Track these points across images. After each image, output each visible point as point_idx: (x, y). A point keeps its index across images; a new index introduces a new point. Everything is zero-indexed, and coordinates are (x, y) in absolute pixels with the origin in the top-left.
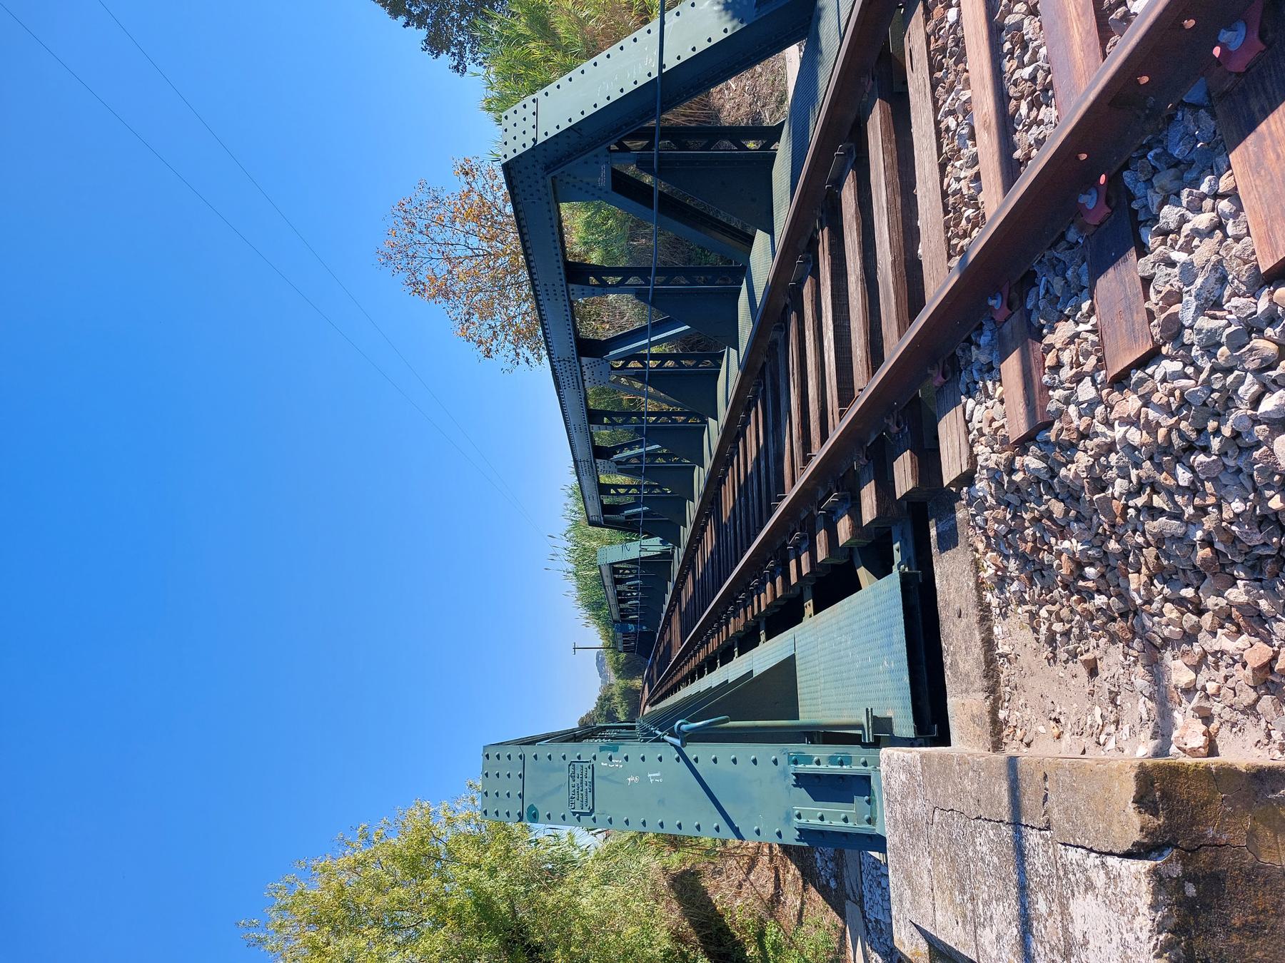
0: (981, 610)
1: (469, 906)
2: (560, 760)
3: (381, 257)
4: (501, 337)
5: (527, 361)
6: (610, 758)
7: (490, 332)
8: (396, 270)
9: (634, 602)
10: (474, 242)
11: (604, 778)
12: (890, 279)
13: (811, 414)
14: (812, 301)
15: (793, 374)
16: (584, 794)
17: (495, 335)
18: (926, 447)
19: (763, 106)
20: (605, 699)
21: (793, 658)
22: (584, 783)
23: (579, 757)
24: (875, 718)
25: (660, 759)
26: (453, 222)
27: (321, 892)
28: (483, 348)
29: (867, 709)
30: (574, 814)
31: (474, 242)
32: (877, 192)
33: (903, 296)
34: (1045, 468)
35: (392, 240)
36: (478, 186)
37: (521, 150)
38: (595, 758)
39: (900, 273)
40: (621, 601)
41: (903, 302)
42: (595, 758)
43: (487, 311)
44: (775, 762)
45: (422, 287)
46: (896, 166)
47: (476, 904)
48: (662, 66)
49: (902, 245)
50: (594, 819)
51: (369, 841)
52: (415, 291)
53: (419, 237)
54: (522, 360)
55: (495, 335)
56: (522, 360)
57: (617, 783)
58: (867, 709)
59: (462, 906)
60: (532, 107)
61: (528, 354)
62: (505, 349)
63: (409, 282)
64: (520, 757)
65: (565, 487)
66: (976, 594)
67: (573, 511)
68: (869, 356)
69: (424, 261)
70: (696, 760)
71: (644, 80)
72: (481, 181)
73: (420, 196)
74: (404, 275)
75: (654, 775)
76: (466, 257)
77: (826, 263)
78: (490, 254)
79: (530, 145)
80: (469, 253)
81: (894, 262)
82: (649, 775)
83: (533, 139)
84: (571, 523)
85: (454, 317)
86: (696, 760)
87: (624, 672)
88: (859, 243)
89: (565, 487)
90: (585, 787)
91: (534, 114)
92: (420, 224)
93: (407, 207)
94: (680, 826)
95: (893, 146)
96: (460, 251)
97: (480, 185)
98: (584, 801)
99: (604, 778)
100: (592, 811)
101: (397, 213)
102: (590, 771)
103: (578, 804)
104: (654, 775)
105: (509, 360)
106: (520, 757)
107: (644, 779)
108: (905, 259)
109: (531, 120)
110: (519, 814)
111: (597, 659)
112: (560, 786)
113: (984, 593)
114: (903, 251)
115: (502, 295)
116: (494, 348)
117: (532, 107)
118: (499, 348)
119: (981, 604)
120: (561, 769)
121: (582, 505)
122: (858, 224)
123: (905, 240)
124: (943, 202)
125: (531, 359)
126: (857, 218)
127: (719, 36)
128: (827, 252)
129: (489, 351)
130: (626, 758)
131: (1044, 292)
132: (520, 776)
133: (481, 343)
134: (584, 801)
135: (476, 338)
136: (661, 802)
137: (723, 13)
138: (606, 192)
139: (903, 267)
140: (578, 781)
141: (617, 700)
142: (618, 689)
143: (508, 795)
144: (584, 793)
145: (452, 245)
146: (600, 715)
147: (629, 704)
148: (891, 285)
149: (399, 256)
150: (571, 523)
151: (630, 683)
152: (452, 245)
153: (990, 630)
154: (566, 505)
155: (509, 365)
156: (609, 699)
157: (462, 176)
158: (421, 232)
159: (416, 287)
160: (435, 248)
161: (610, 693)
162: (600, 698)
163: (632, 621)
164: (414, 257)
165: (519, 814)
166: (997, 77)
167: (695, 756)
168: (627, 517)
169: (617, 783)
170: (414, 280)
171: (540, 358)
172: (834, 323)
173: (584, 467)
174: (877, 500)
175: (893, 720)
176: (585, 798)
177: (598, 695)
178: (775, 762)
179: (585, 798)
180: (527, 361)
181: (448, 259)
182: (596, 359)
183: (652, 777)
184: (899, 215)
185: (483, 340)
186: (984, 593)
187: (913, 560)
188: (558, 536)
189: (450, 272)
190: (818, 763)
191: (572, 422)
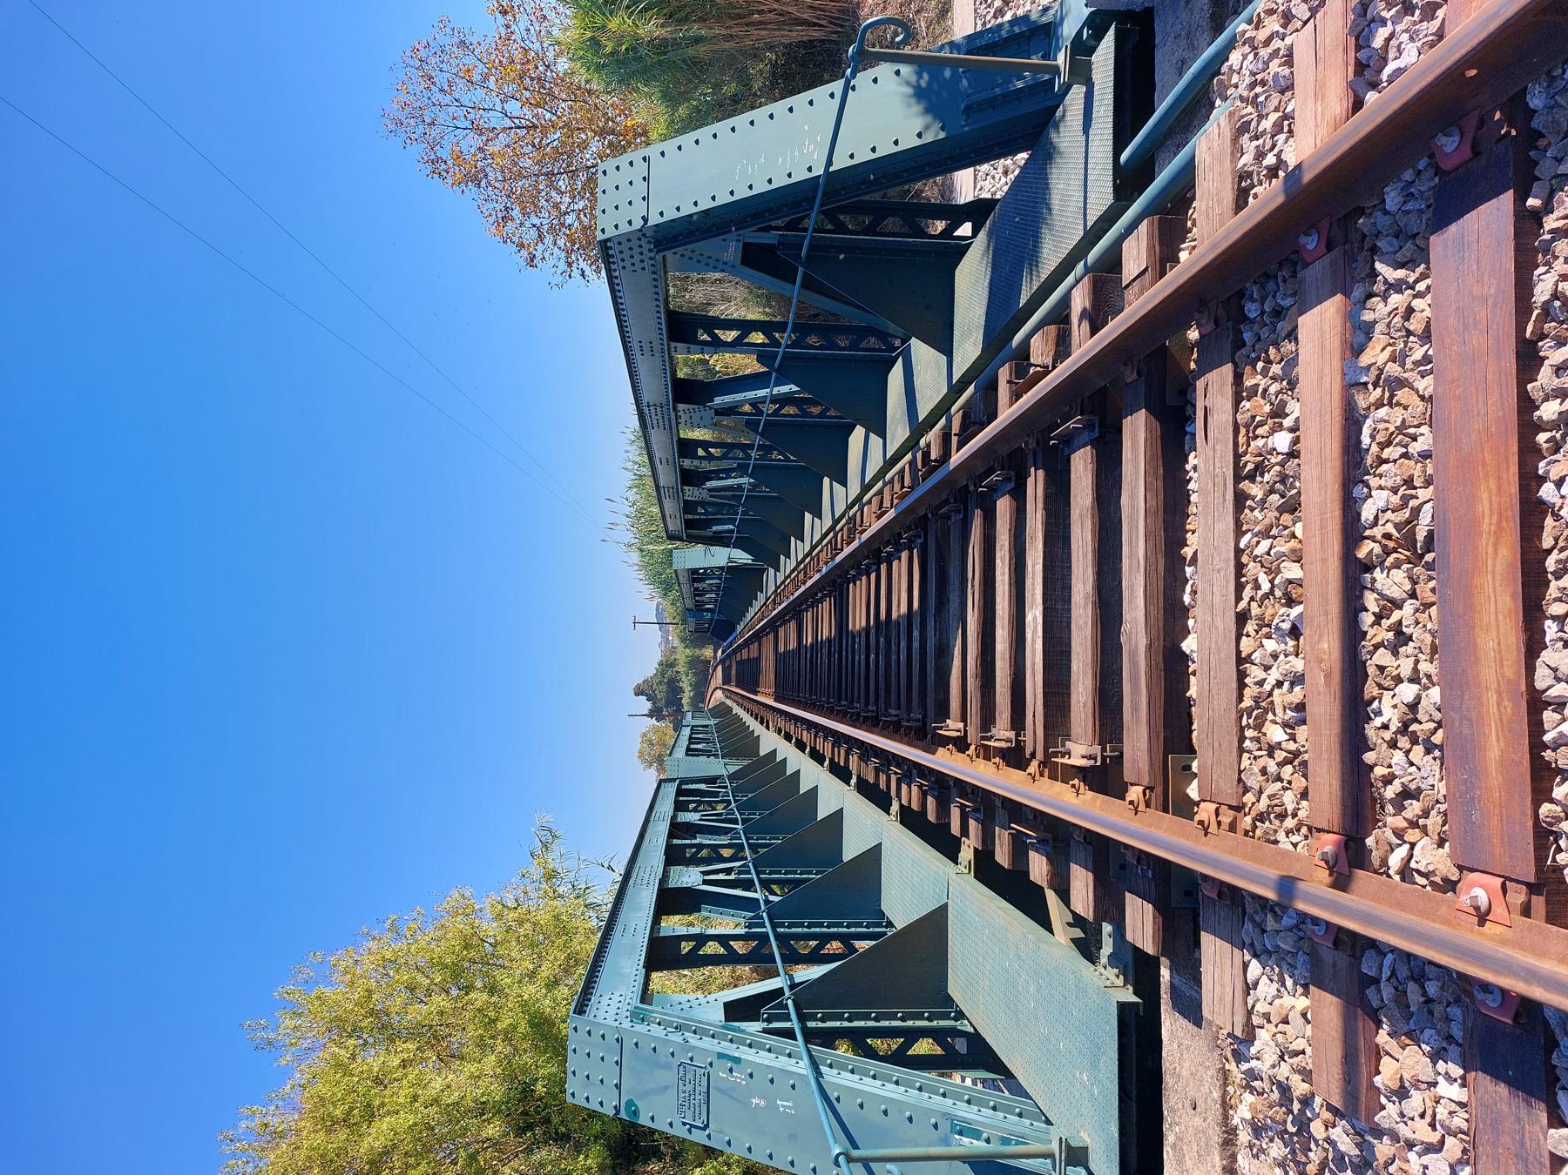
0: (1225, 1132)
1: (523, 1027)
2: (667, 1056)
3: (388, 122)
4: (549, 240)
5: (583, 275)
6: (731, 1070)
7: (534, 233)
8: (408, 141)
9: (715, 581)
10: (513, 107)
11: (720, 1091)
12: (1142, 641)
13: (998, 679)
14: (1010, 530)
15: (973, 586)
16: (697, 1105)
17: (541, 237)
18: (1173, 906)
19: (918, 11)
20: (667, 665)
21: (944, 908)
22: (697, 1092)
23: (691, 1059)
24: (1068, 1146)
25: (793, 1087)
26: (485, 78)
27: (340, 995)
28: (524, 253)
29: (1061, 1139)
30: (685, 1124)
31: (513, 107)
32: (1131, 544)
33: (1158, 695)
34: (1358, 1156)
35: (404, 97)
36: (519, 30)
37: (624, 228)
38: (711, 1064)
39: (1157, 664)
40: (694, 580)
41: (1158, 705)
42: (711, 1064)
43: (529, 204)
44: (936, 1126)
45: (443, 166)
46: (1161, 513)
47: (532, 1024)
48: (829, 162)
49: (1161, 626)
50: (709, 1136)
51: (399, 935)
52: (434, 172)
53: (440, 96)
54: (576, 273)
55: (541, 237)
56: (576, 273)
57: (738, 1100)
58: (1061, 1139)
59: (514, 1027)
60: (641, 168)
61: (583, 265)
62: (553, 254)
63: (426, 159)
64: (617, 1040)
65: (626, 430)
66: (1221, 1110)
67: (636, 463)
68: (1097, 708)
69: (446, 131)
70: (838, 1099)
71: (801, 175)
72: (523, 21)
73: (441, 40)
74: (418, 149)
75: (785, 1103)
76: (504, 130)
77: (1039, 515)
78: (535, 127)
79: (638, 224)
80: (508, 123)
81: (1149, 647)
82: (779, 1102)
83: (643, 218)
84: (634, 477)
85: (487, 213)
86: (838, 1099)
87: (691, 641)
88: (1094, 551)
89: (626, 430)
90: (698, 1097)
91: (644, 179)
92: (441, 79)
93: (423, 53)
94: (771, 1156)
95: (1160, 484)
96: (496, 120)
97: (522, 26)
98: (697, 1112)
99: (720, 1091)
100: (706, 1127)
101: (409, 61)
102: (705, 1080)
103: (689, 1114)
104: (785, 1103)
105: (559, 272)
106: (617, 1040)
107: (772, 1106)
108: (1164, 646)
109: (641, 187)
110: (615, 1107)
111: (657, 609)
112: (667, 1087)
113: (1231, 1112)
114: (1162, 634)
115: (551, 185)
116: (538, 254)
117: (641, 168)
118: (547, 255)
119: (1226, 1126)
120: (667, 1067)
121: (646, 458)
122: (1093, 523)
123: (1165, 620)
124: (1237, 667)
125: (588, 272)
126: (1093, 515)
127: (910, 142)
128: (1040, 505)
129: (533, 258)
130: (751, 1075)
131: (1389, 974)
132: (617, 1063)
133: (521, 246)
134: (697, 1112)
135: (516, 239)
136: (792, 1137)
137: (913, 101)
138: (733, 266)
139: (1161, 658)
140: (689, 1087)
141: (681, 668)
142: (683, 657)
143: (602, 1081)
144: (697, 1102)
145: (484, 110)
146: (660, 682)
147: (695, 674)
148: (1142, 656)
149: (412, 121)
150: (634, 477)
151: (697, 652)
152: (484, 110)
153: (1233, 1158)
154: (627, 452)
155: (559, 279)
156: (672, 665)
157: (499, 16)
158: (442, 90)
159: (436, 165)
160: (461, 112)
161: (673, 658)
162: (661, 664)
163: (708, 610)
164: (433, 124)
165: (615, 1107)
166: (1349, 627)
167: (836, 1094)
168: (714, 533)
169: (738, 1100)
170: (433, 157)
171: (598, 271)
172: (1044, 604)
173: (653, 417)
174: (1095, 901)
175: (1090, 1150)
176: (697, 1110)
177: (658, 661)
178: (936, 1126)
179: (697, 1110)
180: (583, 275)
181: (480, 131)
182: (696, 407)
183: (782, 1106)
184: (1161, 584)
185: (526, 242)
186: (1231, 1112)
187: (1130, 965)
188: (618, 499)
189: (481, 149)
190: (988, 1141)
191: (635, 335)
